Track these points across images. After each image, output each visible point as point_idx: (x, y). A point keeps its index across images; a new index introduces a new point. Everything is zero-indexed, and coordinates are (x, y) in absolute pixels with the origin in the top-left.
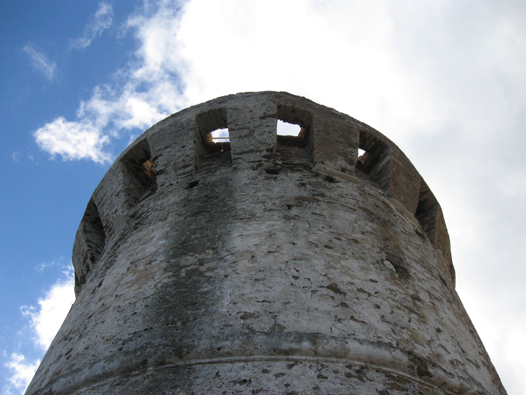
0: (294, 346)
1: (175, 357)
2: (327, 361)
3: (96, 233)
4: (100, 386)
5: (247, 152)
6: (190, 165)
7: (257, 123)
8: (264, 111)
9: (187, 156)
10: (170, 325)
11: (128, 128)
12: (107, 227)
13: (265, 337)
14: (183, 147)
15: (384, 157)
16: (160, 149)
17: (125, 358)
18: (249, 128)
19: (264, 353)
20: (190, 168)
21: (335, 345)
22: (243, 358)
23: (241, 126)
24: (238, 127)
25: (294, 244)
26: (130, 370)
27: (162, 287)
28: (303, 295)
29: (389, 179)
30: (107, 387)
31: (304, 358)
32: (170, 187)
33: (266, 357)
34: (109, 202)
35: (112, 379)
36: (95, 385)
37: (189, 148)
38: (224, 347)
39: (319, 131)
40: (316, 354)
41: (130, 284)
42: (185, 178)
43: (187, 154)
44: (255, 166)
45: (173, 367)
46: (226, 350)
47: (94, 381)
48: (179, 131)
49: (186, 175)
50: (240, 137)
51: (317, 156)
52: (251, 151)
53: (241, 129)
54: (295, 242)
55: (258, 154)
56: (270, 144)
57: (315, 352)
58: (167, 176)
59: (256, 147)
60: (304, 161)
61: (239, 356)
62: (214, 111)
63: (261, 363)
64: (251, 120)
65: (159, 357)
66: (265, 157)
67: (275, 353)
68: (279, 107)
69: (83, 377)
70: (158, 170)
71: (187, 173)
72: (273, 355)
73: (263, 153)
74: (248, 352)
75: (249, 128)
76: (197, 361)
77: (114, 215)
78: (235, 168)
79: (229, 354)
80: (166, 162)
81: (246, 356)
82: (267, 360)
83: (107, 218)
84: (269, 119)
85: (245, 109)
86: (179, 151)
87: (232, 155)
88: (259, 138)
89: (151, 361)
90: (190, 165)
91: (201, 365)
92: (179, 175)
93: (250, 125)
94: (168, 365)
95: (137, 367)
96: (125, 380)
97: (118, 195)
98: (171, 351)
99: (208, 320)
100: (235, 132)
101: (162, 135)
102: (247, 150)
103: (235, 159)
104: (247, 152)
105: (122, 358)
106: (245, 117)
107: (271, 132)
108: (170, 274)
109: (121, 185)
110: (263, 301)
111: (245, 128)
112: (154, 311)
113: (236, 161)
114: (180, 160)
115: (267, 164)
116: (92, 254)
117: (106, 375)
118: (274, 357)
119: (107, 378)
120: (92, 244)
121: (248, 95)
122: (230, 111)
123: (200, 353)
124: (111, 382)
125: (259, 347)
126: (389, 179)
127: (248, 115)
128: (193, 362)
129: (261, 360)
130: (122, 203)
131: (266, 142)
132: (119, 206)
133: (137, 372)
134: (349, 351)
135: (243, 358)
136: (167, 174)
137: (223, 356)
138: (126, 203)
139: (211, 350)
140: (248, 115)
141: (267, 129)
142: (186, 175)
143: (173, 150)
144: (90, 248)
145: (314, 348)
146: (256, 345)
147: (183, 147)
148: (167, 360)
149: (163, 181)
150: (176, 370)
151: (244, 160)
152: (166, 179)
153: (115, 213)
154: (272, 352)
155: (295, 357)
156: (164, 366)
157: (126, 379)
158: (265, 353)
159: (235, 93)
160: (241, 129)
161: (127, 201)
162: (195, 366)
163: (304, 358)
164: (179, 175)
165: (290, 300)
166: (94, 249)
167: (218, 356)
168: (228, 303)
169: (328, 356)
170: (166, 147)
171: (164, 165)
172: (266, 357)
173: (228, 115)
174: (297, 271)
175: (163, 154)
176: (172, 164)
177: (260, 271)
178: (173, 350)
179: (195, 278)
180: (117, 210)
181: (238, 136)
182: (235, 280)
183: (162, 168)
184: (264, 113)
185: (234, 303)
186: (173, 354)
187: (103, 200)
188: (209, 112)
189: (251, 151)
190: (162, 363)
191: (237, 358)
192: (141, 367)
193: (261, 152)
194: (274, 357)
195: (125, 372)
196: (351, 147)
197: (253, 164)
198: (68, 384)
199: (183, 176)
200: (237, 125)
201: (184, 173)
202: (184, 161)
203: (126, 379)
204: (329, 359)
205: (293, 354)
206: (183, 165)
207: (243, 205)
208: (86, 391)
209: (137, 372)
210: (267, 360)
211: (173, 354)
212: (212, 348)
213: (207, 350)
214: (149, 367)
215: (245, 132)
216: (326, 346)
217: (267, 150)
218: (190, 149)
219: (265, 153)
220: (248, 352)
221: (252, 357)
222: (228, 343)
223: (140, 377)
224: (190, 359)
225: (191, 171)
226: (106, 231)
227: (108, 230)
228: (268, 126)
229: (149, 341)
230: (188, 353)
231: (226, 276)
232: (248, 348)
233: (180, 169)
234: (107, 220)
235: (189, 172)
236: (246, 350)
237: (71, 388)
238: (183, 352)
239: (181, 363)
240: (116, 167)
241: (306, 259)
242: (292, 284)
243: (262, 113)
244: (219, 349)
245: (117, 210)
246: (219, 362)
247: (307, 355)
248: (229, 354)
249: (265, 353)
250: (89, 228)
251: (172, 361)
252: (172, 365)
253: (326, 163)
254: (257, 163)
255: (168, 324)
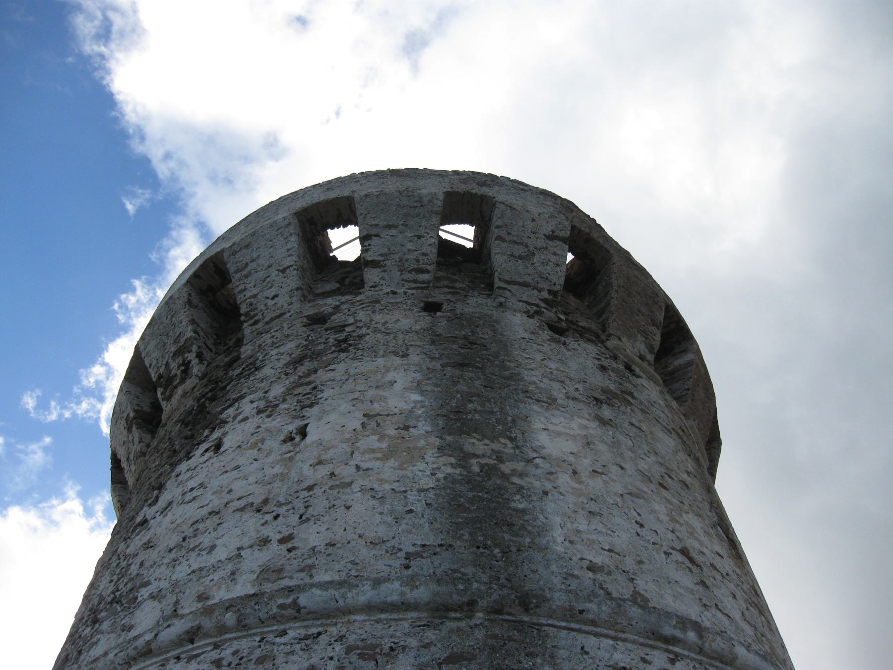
0: (678, 633)
1: (518, 608)
2: (711, 665)
3: (205, 311)
4: (391, 619)
5: (520, 284)
6: (428, 272)
7: (541, 243)
8: (553, 228)
9: (424, 254)
10: (482, 550)
11: (108, 78)
12: (247, 314)
13: (639, 610)
14: (419, 237)
15: (681, 352)
16: (376, 225)
17: (439, 588)
18: (526, 246)
19: (639, 633)
20: (426, 277)
21: (723, 646)
22: (611, 633)
23: (515, 239)
24: (511, 238)
25: (622, 468)
26: (447, 608)
27: (445, 478)
28: (656, 556)
29: (688, 389)
30: (406, 625)
31: (686, 653)
32: (391, 295)
33: (641, 640)
34: (261, 275)
35: (414, 614)
36: (383, 616)
37: (429, 243)
38: (588, 611)
39: (619, 286)
40: (701, 651)
41: (379, 455)
42: (420, 291)
43: (424, 251)
44: (532, 312)
45: (514, 622)
46: (591, 616)
47: (382, 611)
48: (415, 207)
49: (418, 285)
50: (512, 255)
51: (613, 327)
52: (525, 285)
53: (515, 242)
54: (624, 466)
55: (535, 292)
56: (555, 284)
57: (701, 649)
58: (384, 274)
59: (533, 279)
60: (593, 326)
61: (607, 629)
62: (473, 196)
63: (635, 646)
64: (532, 235)
65: (495, 601)
66: (544, 300)
67: (653, 637)
68: (573, 228)
69: (362, 599)
70: (370, 259)
71: (420, 283)
72: (650, 639)
73: (542, 293)
74: (619, 627)
75: (526, 246)
76: (549, 622)
77: (270, 303)
78: (501, 304)
79: (593, 623)
80: (385, 250)
81: (616, 631)
82: (642, 644)
83: (252, 300)
84: (558, 242)
85: (526, 214)
86: (411, 241)
87: (496, 280)
88: (540, 268)
89: (482, 603)
90: (428, 272)
91: (555, 630)
92: (406, 281)
93: (529, 241)
94: (507, 617)
95: (459, 608)
96: (437, 621)
97: (283, 271)
98: (513, 596)
99: (540, 559)
100: (505, 245)
101: (384, 204)
102: (519, 280)
103: (499, 288)
104: (520, 284)
105: (433, 587)
106: (523, 226)
107: (558, 265)
108: (452, 460)
109: (293, 258)
110: (609, 550)
111: (522, 244)
112: (446, 519)
113: (501, 291)
114: (411, 256)
115: (549, 314)
116: (199, 347)
117: (405, 606)
118: (651, 642)
119: (406, 610)
120: (199, 330)
121: (521, 187)
122: (502, 207)
123: (555, 611)
124: (412, 618)
125: (634, 623)
126: (688, 389)
127: (529, 225)
128: (543, 621)
129: (634, 642)
130: (290, 288)
131: (549, 278)
132: (284, 291)
133: (458, 615)
134: (737, 658)
135: (611, 633)
136: (384, 271)
137: (585, 623)
138: (300, 291)
139: (570, 610)
140: (529, 225)
141: (553, 259)
142: (418, 285)
143: (400, 236)
144: (197, 336)
145: (700, 642)
146: (631, 619)
147: (419, 237)
148: (507, 609)
149: (377, 279)
150: (519, 625)
151: (513, 295)
152: (383, 278)
153: (273, 298)
154: (650, 634)
155: (677, 649)
156: (501, 617)
157: (440, 621)
158: (640, 633)
159: (499, 175)
160: (515, 242)
161: (301, 289)
162: (546, 628)
163: (686, 653)
164: (406, 281)
165: (644, 560)
166: (202, 340)
167: (578, 622)
168: (562, 539)
169: (712, 658)
170: (389, 227)
171: (382, 255)
172: (641, 640)
173: (497, 212)
174: (639, 515)
175: (382, 235)
176: (396, 257)
177: (592, 499)
178: (516, 596)
179: (498, 482)
180: (276, 296)
181: (509, 253)
182: (559, 502)
183: (377, 258)
184: (553, 231)
185: (571, 542)
186: (517, 602)
187: (248, 269)
188: (464, 194)
189: (525, 285)
190: (499, 612)
191: (605, 631)
192: (466, 608)
193: (539, 291)
194: (651, 642)
195: (438, 609)
196: (653, 325)
197: (529, 307)
198: (333, 603)
199: (413, 285)
200: (509, 234)
201: (415, 281)
202: (418, 261)
203: (440, 621)
204: (713, 662)
205: (673, 645)
206: (416, 266)
207: (533, 376)
208: (364, 621)
209: (458, 615)
210: (642, 644)
211: (517, 602)
212: (571, 608)
213: (565, 609)
214: (478, 611)
215: (520, 250)
216: (713, 644)
217: (550, 292)
218: (430, 245)
219: (545, 295)
220: (619, 627)
221: (623, 636)
222: (592, 606)
223: (463, 624)
224: (539, 615)
225: (428, 282)
226: (245, 321)
227: (252, 322)
228: (555, 254)
229: (456, 566)
230: (537, 607)
231: (546, 493)
232: (620, 621)
233: (410, 272)
234: (251, 304)
235: (423, 282)
236: (617, 624)
237: (338, 610)
238: (531, 603)
239: (526, 619)
240: (286, 222)
241: (644, 499)
242: (638, 535)
243: (549, 229)
244: (581, 612)
245: (276, 296)
246: (579, 631)
247: (689, 650)
248: (593, 623)
249: (640, 633)
250: (195, 300)
251: (513, 611)
252: (514, 618)
253: (623, 339)
254: (535, 308)
255: (478, 547)
